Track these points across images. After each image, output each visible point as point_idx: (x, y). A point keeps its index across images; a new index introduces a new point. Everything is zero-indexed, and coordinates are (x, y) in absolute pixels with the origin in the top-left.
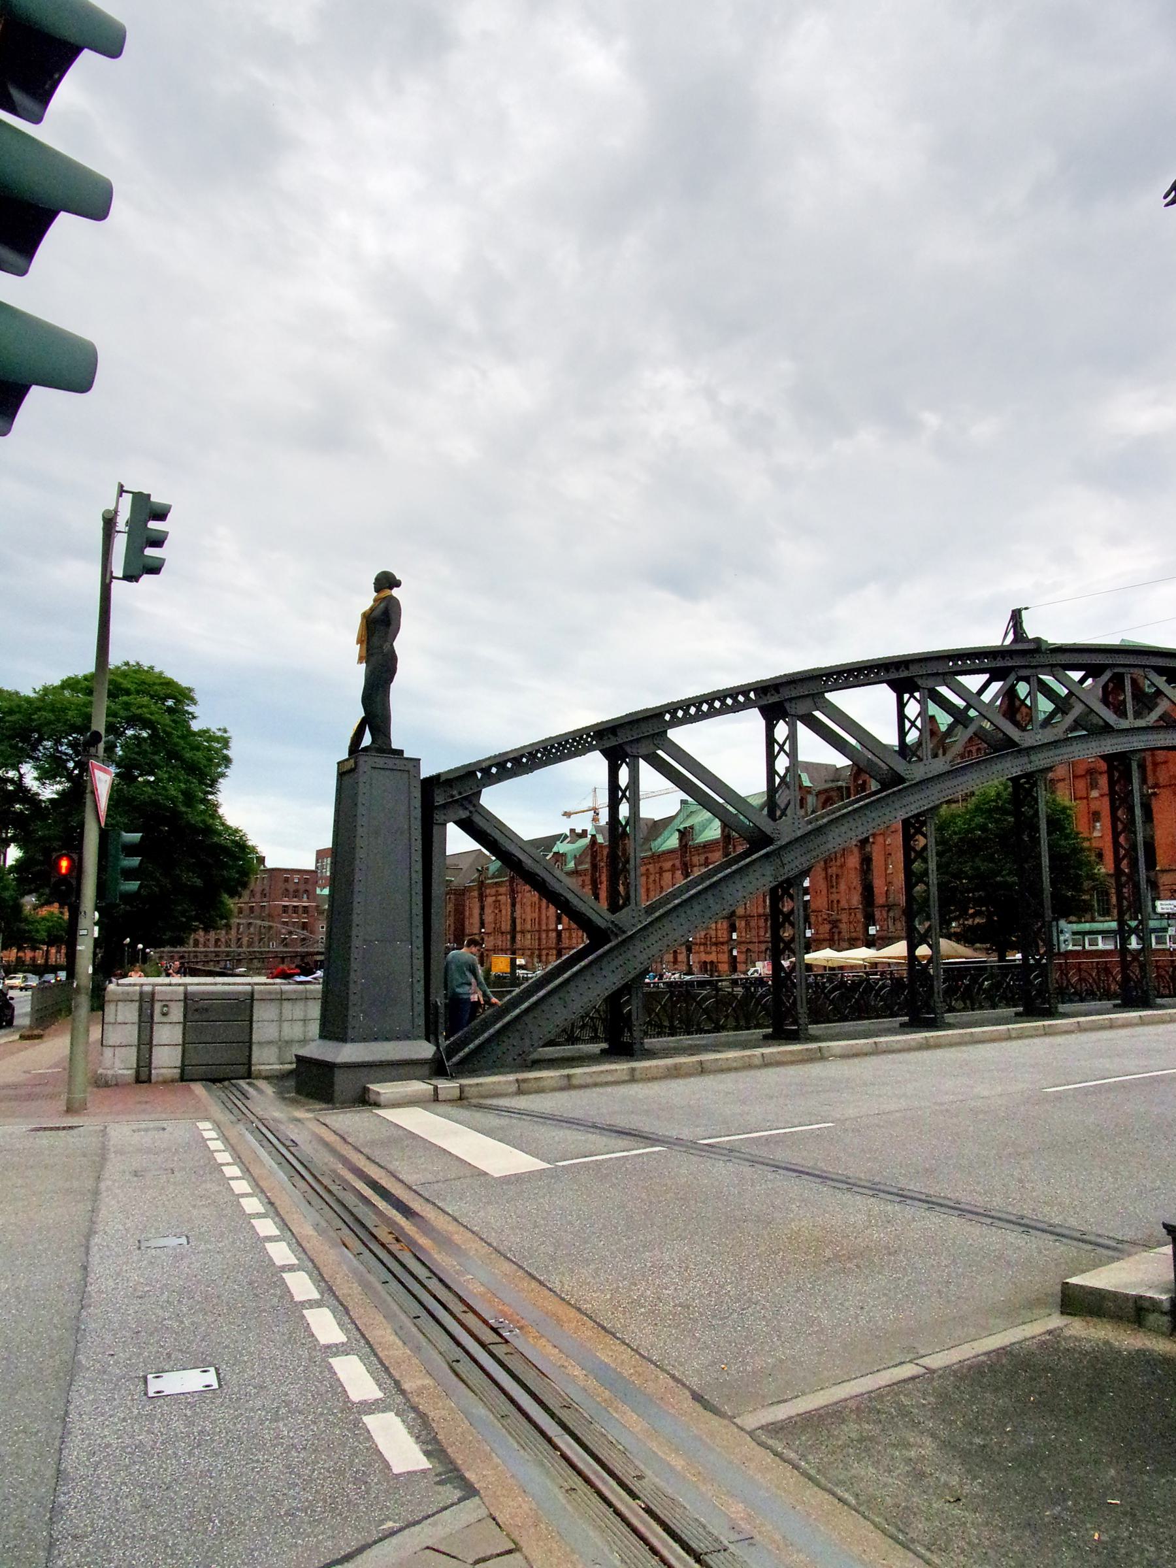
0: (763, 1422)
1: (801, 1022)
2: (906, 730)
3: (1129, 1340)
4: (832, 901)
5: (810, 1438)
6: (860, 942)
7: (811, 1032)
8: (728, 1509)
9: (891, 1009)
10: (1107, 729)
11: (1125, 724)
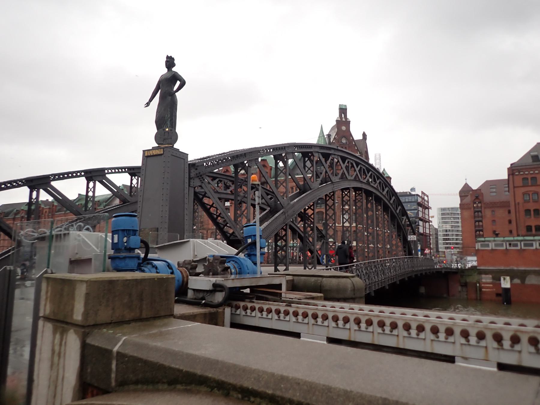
2: (136, 184)
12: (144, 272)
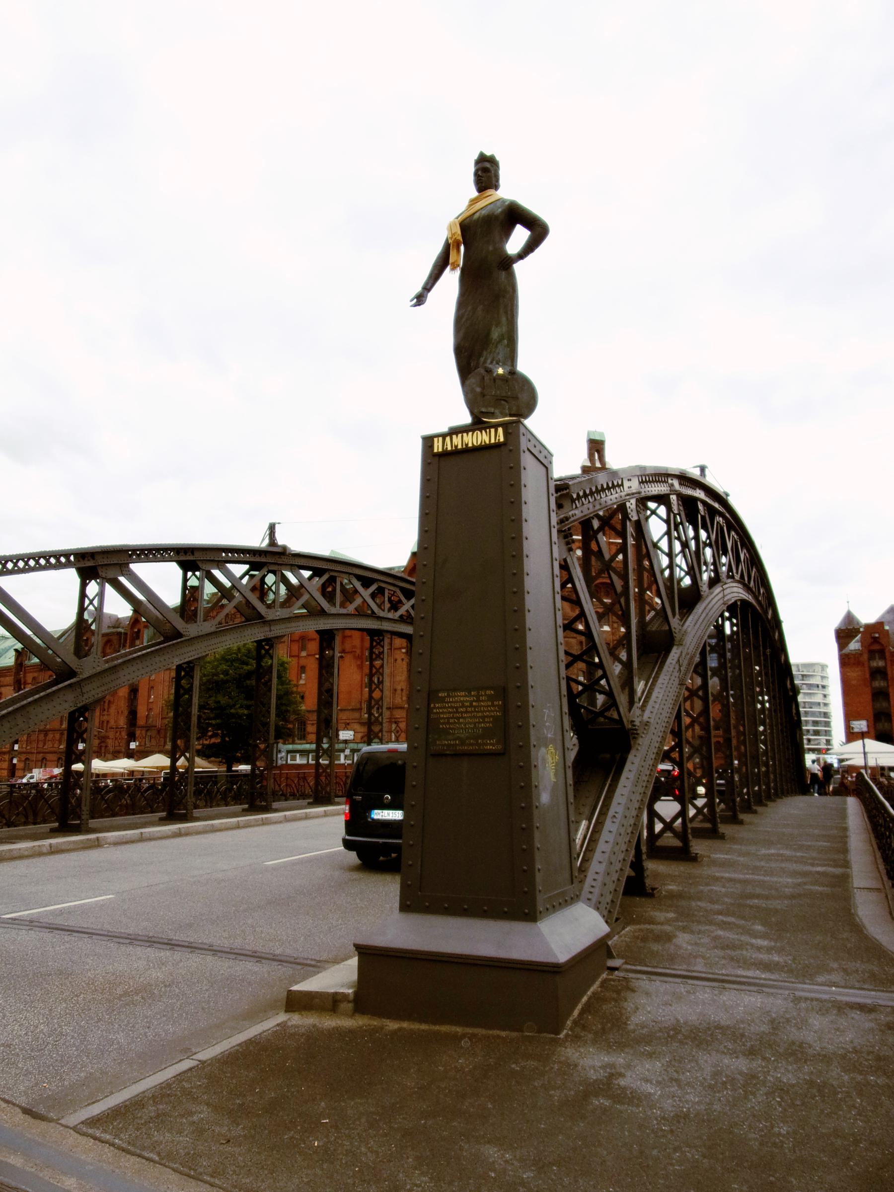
0: (83, 1118)
1: (83, 817)
3: (329, 1022)
4: (103, 722)
5: (120, 1122)
6: (121, 755)
7: (273, 807)
8: (63, 1184)
9: (152, 807)
10: (322, 613)
11: (333, 610)
12: (724, 839)
